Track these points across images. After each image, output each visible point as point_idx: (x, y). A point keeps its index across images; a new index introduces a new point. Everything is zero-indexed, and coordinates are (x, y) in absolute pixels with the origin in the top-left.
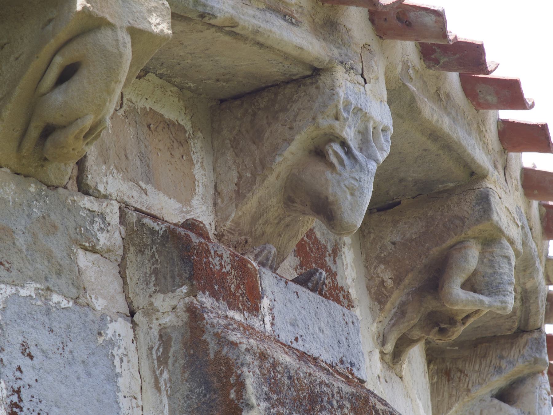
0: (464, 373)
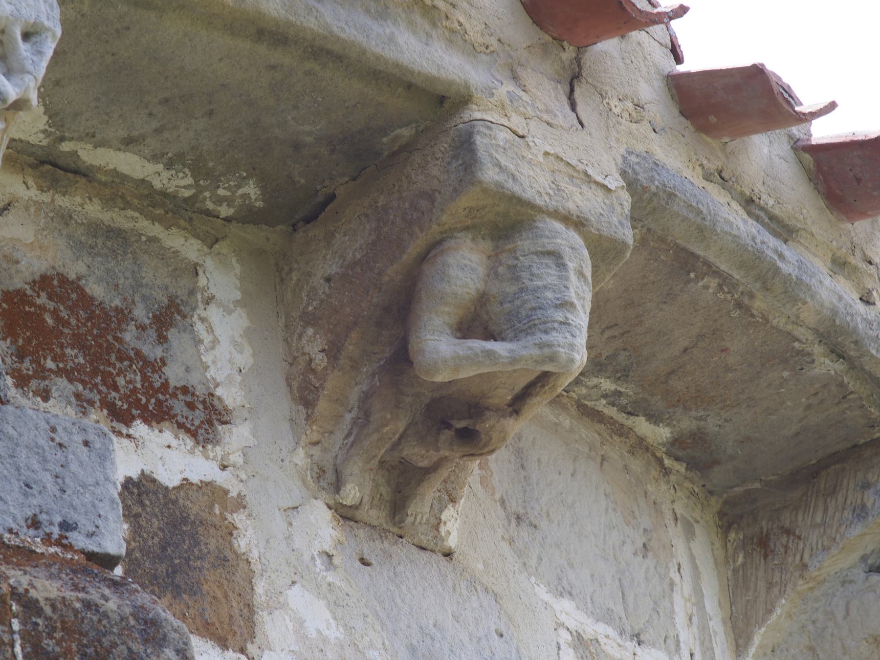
0: (794, 534)
